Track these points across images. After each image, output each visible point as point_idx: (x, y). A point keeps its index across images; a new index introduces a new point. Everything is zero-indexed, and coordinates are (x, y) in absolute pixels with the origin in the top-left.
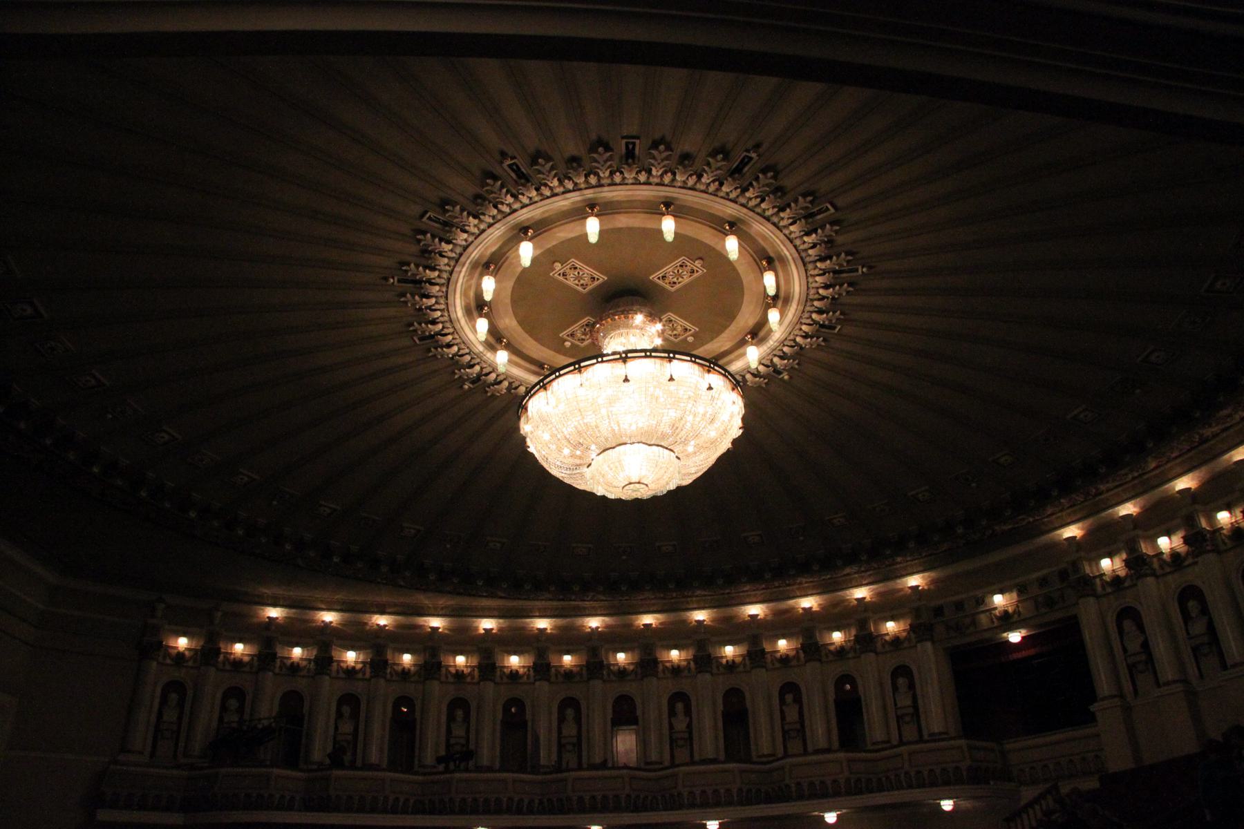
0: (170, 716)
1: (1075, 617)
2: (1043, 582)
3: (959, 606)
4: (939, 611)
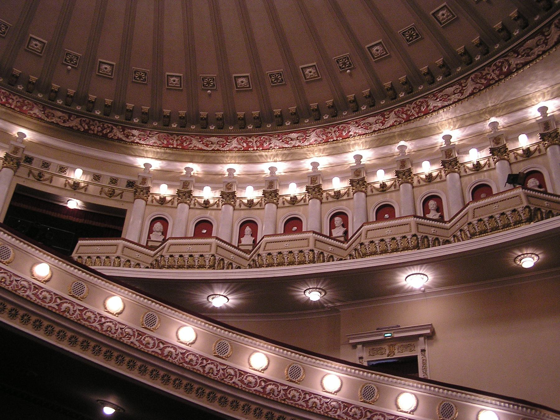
1: (123, 212)
2: (114, 181)
3: (46, 165)
4: (29, 160)
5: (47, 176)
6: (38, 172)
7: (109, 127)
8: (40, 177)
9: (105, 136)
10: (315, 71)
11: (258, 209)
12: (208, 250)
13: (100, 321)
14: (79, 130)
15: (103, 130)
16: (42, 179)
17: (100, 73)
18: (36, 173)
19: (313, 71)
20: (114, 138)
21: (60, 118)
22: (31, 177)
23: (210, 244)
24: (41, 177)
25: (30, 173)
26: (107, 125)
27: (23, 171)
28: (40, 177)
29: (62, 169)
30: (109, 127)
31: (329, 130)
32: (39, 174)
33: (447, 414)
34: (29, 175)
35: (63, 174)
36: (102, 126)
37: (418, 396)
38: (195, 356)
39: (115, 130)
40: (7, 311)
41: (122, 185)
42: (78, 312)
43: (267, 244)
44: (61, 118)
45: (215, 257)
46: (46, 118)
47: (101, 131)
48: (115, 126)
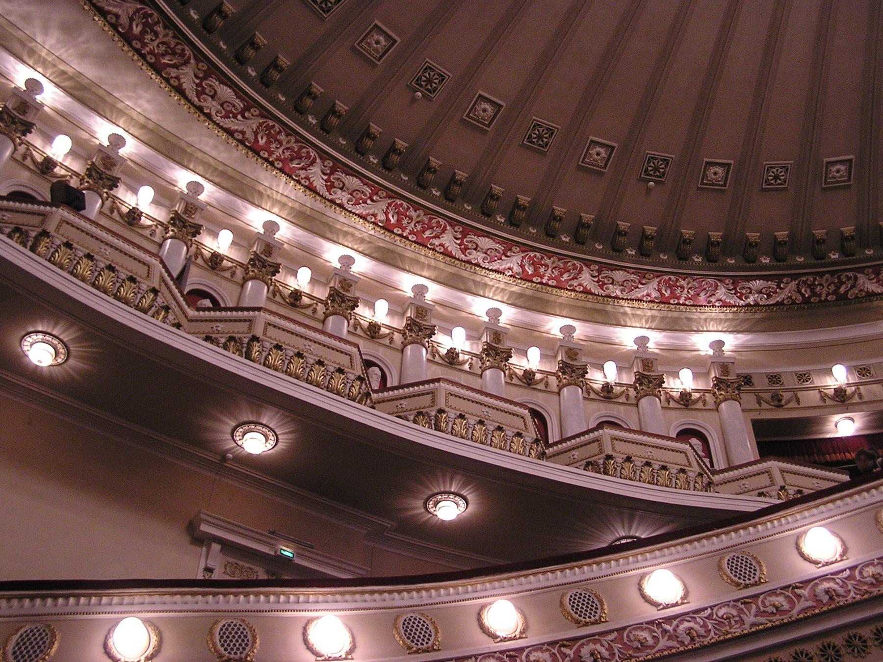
4: (747, 380)
5: (786, 396)
6: (770, 394)
7: (849, 278)
8: (777, 401)
9: (842, 298)
10: (605, 156)
11: (623, 404)
12: (768, 483)
13: (665, 631)
14: (794, 303)
15: (838, 288)
16: (783, 402)
17: (829, 183)
18: (767, 396)
19: (603, 155)
20: (859, 296)
21: (760, 292)
22: (765, 406)
23: (767, 472)
24: (780, 400)
26: (847, 276)
29: (803, 377)
30: (849, 278)
31: (548, 262)
32: (772, 397)
33: (235, 645)
34: (760, 404)
35: (808, 384)
36: (836, 281)
37: (159, 624)
38: (541, 650)
39: (862, 279)
40: (843, 651)
42: (617, 646)
43: (683, 455)
44: (764, 291)
45: (786, 490)
46: (739, 300)
47: (836, 292)
48: (859, 273)
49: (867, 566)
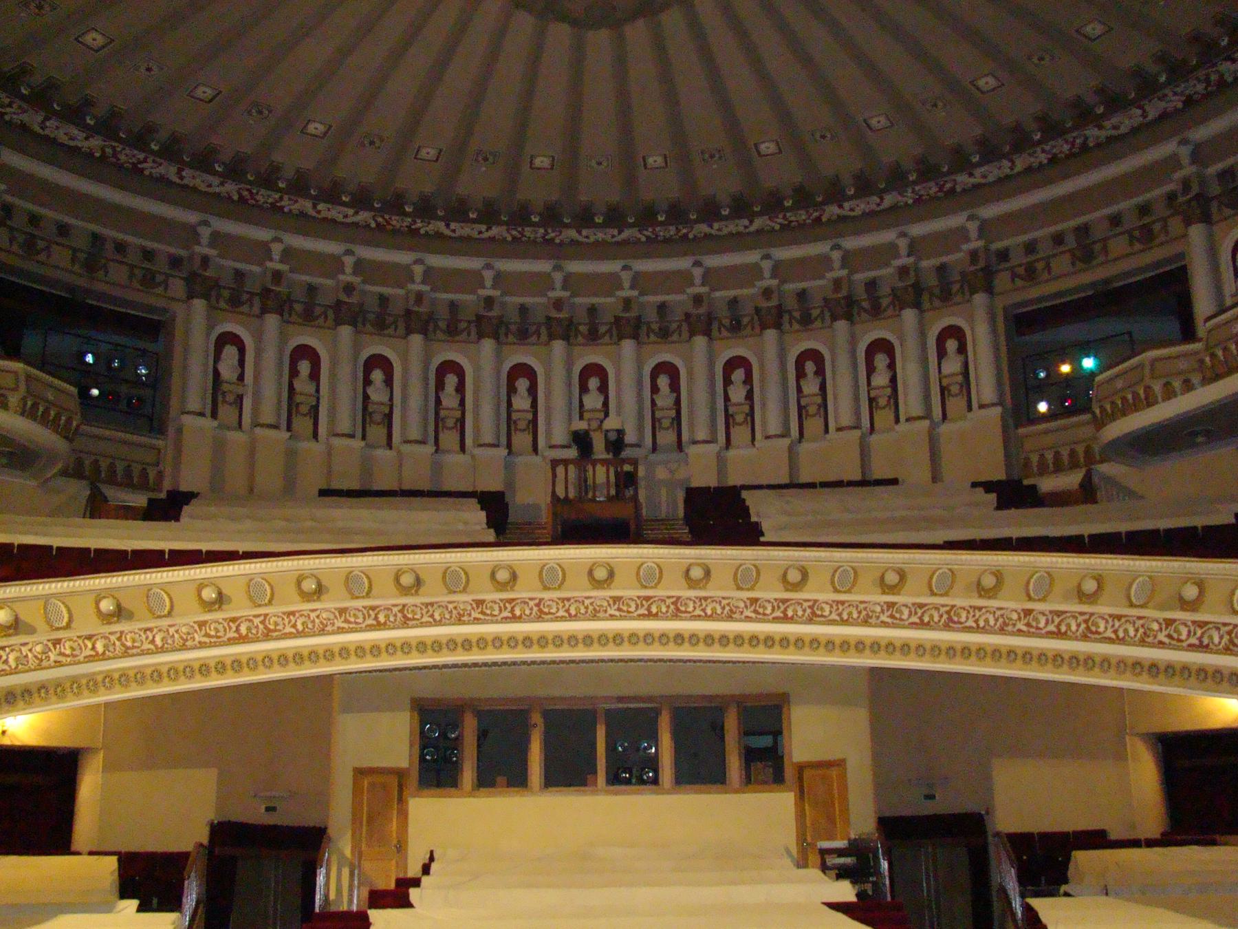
0: (881, 379)
18: (1021, 271)
25: (1014, 276)
27: (1002, 281)
28: (1031, 274)
41: (1161, 210)
49: (275, 616)
